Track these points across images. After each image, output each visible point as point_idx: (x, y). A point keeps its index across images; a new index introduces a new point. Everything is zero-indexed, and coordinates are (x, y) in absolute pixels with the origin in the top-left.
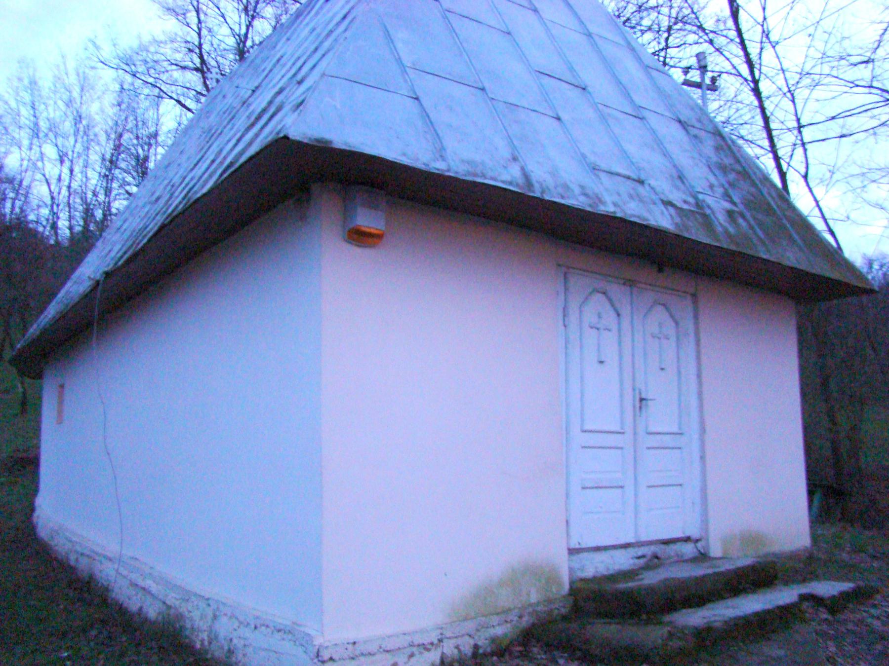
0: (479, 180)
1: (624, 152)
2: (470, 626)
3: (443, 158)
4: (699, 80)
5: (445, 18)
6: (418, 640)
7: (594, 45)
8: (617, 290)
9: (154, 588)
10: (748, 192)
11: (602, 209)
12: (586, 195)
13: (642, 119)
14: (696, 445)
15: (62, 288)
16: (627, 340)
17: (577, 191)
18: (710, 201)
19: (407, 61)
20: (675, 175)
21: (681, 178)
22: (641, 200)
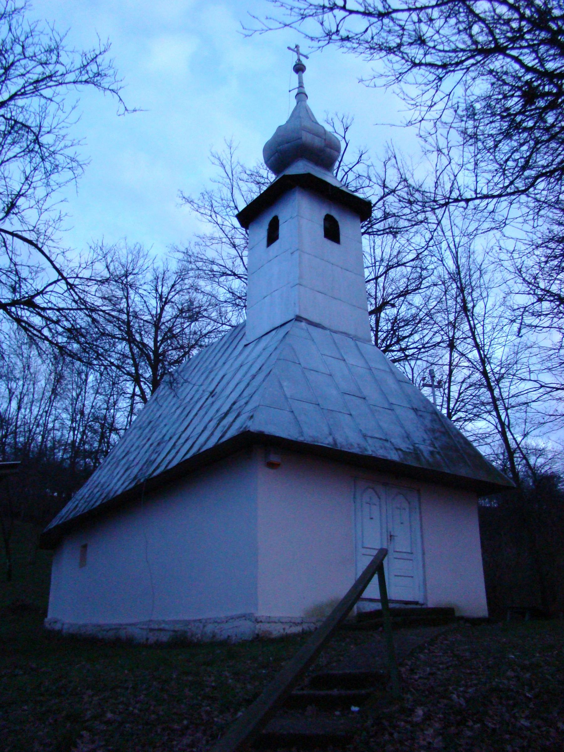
0: (316, 444)
1: (379, 426)
3: (302, 436)
5: (303, 373)
7: (372, 374)
11: (366, 453)
12: (360, 448)
13: (392, 410)
14: (420, 558)
15: (63, 507)
17: (356, 446)
18: (422, 447)
19: (288, 395)
20: (405, 435)
22: (386, 449)
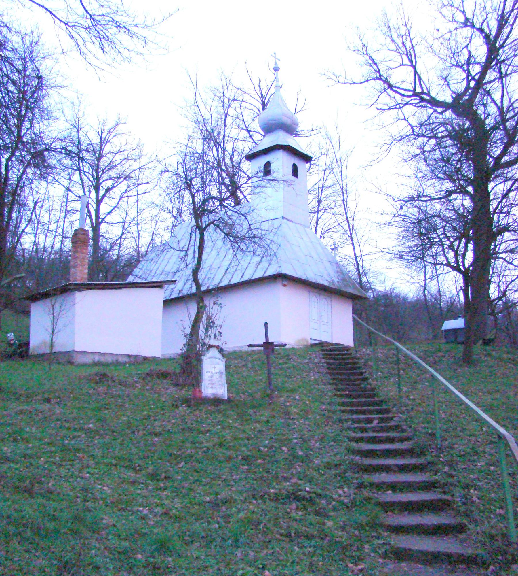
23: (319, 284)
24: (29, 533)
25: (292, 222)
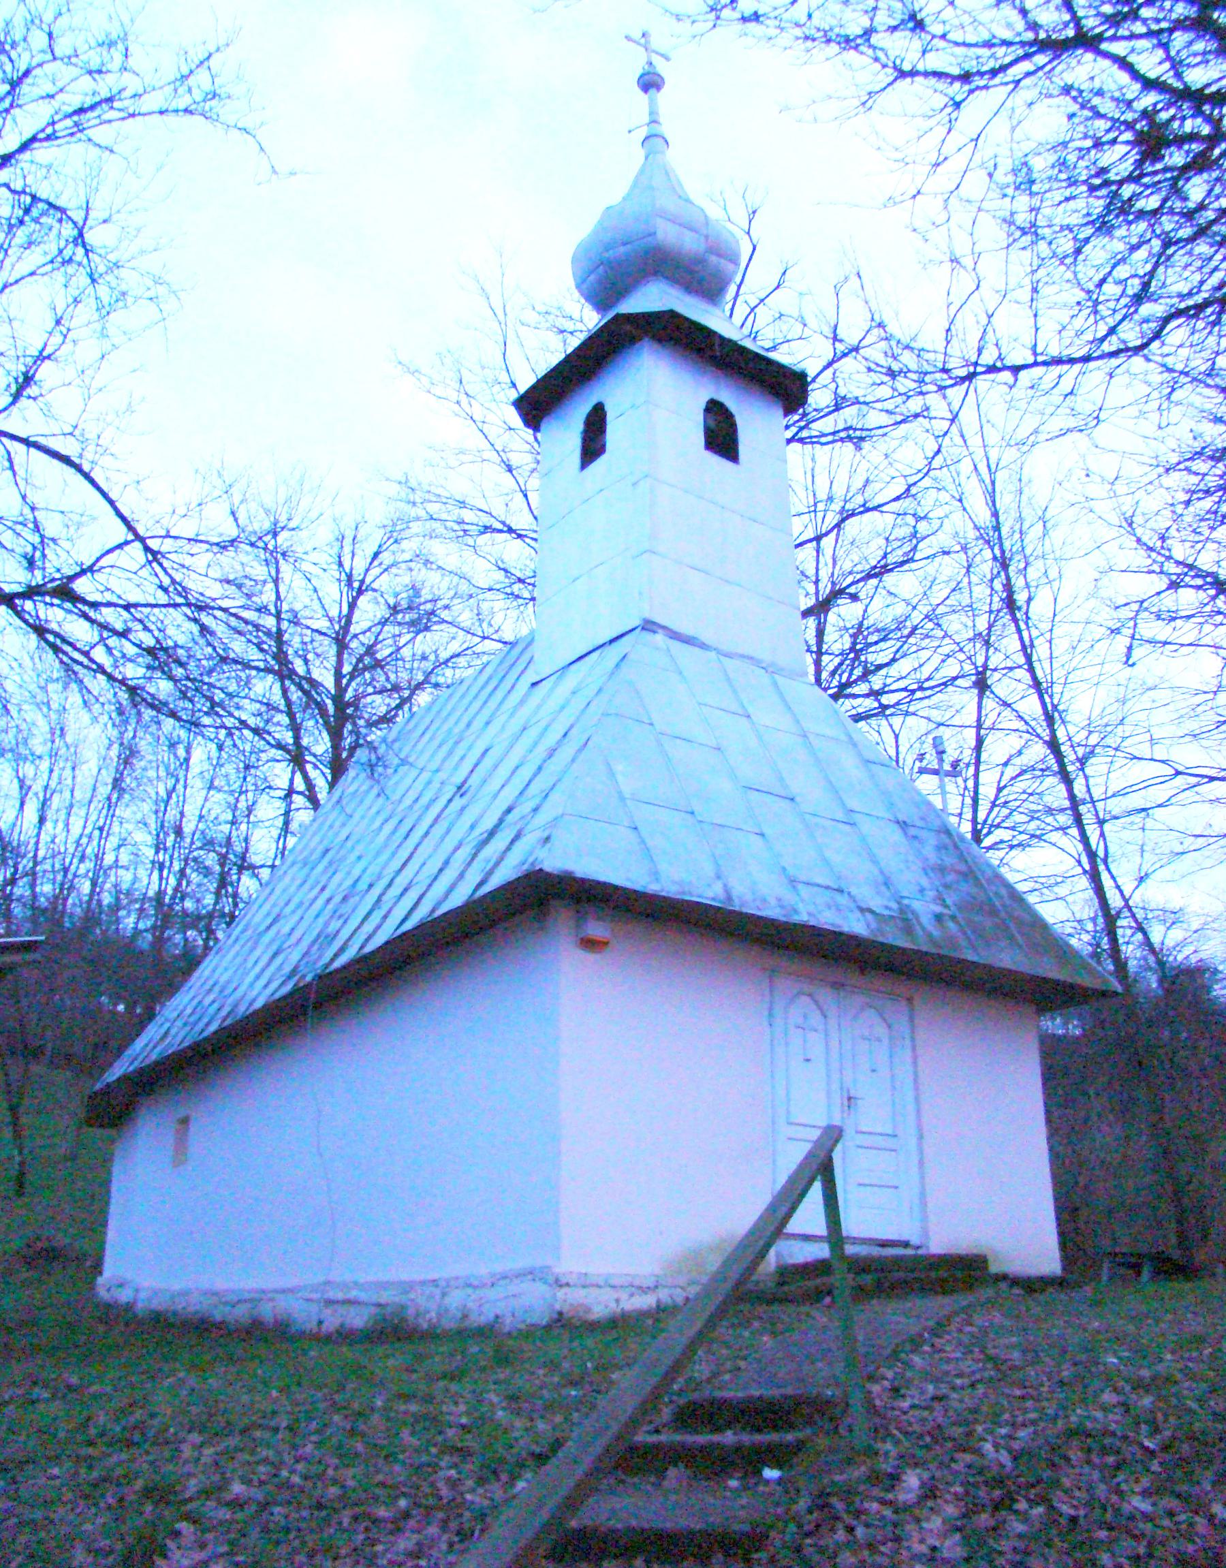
2: (682, 1281)
4: (937, 767)
6: (637, 1283)
8: (826, 995)
9: (363, 1296)
10: (968, 894)
11: (796, 918)
12: (782, 907)
13: (852, 824)
16: (834, 1043)
17: (773, 902)
18: (917, 905)
20: (880, 879)
21: (887, 883)
23: (815, 933)
24: (959, 1274)
25: (703, 646)
